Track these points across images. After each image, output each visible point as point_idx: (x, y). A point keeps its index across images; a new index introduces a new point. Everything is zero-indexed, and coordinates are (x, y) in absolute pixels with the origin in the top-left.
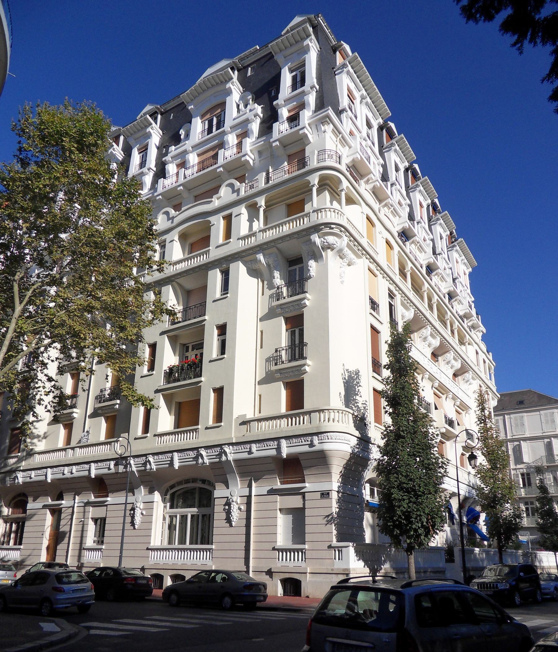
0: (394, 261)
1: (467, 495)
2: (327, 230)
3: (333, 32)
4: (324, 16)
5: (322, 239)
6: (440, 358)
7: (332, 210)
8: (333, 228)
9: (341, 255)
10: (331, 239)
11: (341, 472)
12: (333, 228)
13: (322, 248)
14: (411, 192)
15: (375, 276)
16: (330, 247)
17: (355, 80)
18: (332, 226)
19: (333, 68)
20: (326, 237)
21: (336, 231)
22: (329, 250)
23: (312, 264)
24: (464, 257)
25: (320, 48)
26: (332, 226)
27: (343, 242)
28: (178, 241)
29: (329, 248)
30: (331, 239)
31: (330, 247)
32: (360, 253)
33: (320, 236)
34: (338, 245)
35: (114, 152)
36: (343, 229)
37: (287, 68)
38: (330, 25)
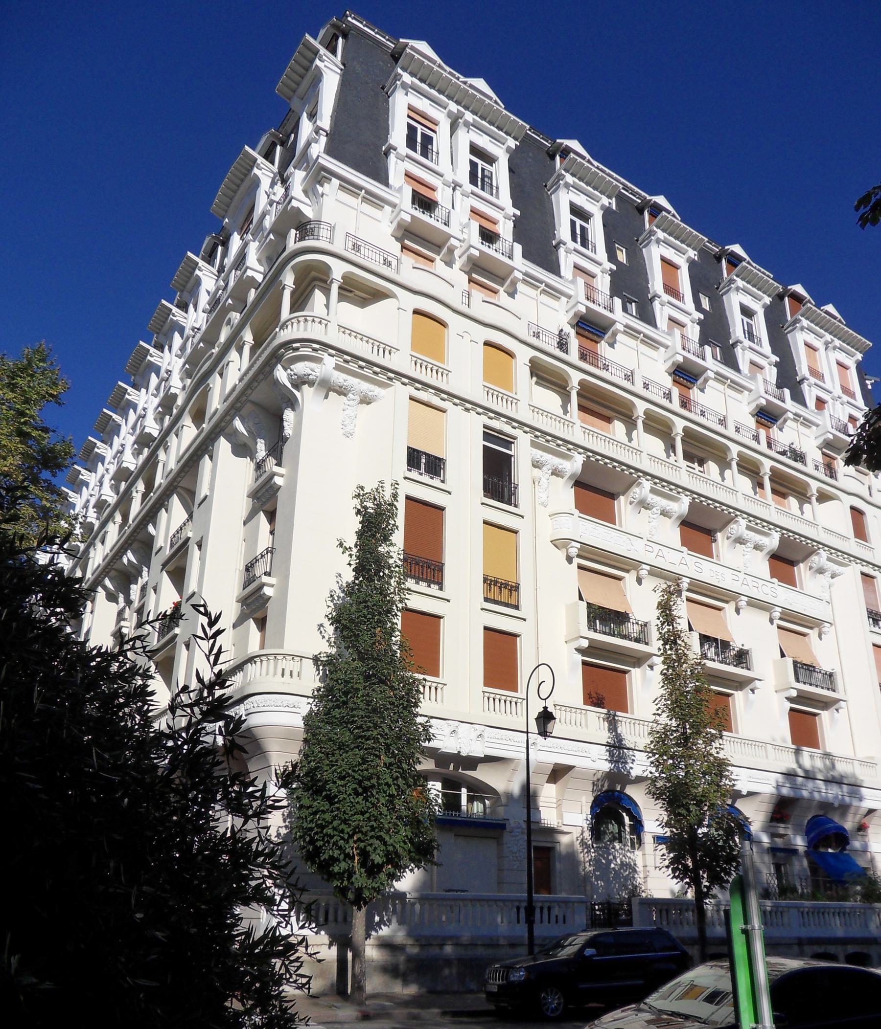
0: (852, 379)
1: (785, 791)
2: (291, 354)
3: (384, 29)
4: (353, 11)
5: (289, 371)
6: (719, 535)
7: (317, 320)
8: (297, 349)
9: (328, 387)
10: (300, 368)
11: (300, 751)
12: (297, 349)
13: (293, 385)
14: (645, 247)
15: (444, 411)
16: (300, 382)
17: (428, 92)
18: (294, 345)
19: (383, 88)
20: (292, 367)
21: (305, 351)
22: (305, 387)
23: (289, 415)
24: (829, 337)
25: (344, 64)
26: (294, 345)
27: (328, 365)
28: (192, 425)
29: (304, 383)
30: (300, 368)
31: (300, 382)
32: (382, 378)
33: (286, 366)
34: (318, 374)
35: (175, 319)
36: (317, 346)
37: (305, 115)
38: (373, 22)
